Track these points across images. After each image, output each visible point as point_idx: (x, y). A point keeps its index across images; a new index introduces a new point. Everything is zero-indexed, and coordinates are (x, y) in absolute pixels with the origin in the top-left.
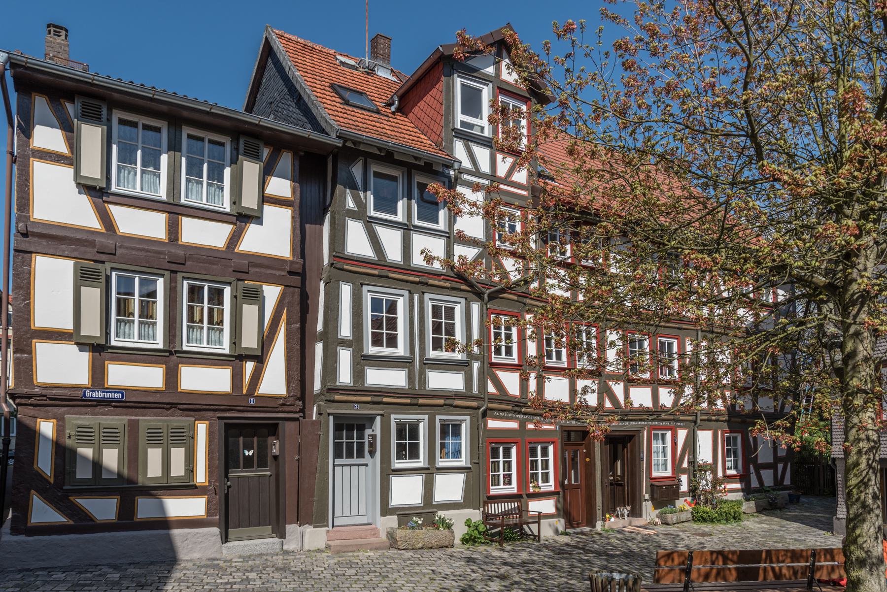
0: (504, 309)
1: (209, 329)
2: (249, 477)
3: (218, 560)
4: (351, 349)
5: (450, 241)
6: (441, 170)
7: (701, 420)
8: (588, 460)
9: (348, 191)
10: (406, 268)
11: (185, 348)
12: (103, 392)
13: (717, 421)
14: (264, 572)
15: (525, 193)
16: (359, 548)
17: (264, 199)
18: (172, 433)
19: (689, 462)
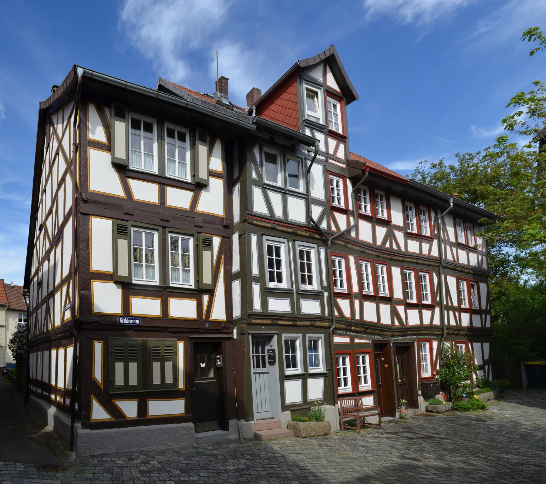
0: (338, 252)
4: (259, 284)
8: (386, 366)
10: (285, 222)
12: (129, 319)
15: (344, 166)
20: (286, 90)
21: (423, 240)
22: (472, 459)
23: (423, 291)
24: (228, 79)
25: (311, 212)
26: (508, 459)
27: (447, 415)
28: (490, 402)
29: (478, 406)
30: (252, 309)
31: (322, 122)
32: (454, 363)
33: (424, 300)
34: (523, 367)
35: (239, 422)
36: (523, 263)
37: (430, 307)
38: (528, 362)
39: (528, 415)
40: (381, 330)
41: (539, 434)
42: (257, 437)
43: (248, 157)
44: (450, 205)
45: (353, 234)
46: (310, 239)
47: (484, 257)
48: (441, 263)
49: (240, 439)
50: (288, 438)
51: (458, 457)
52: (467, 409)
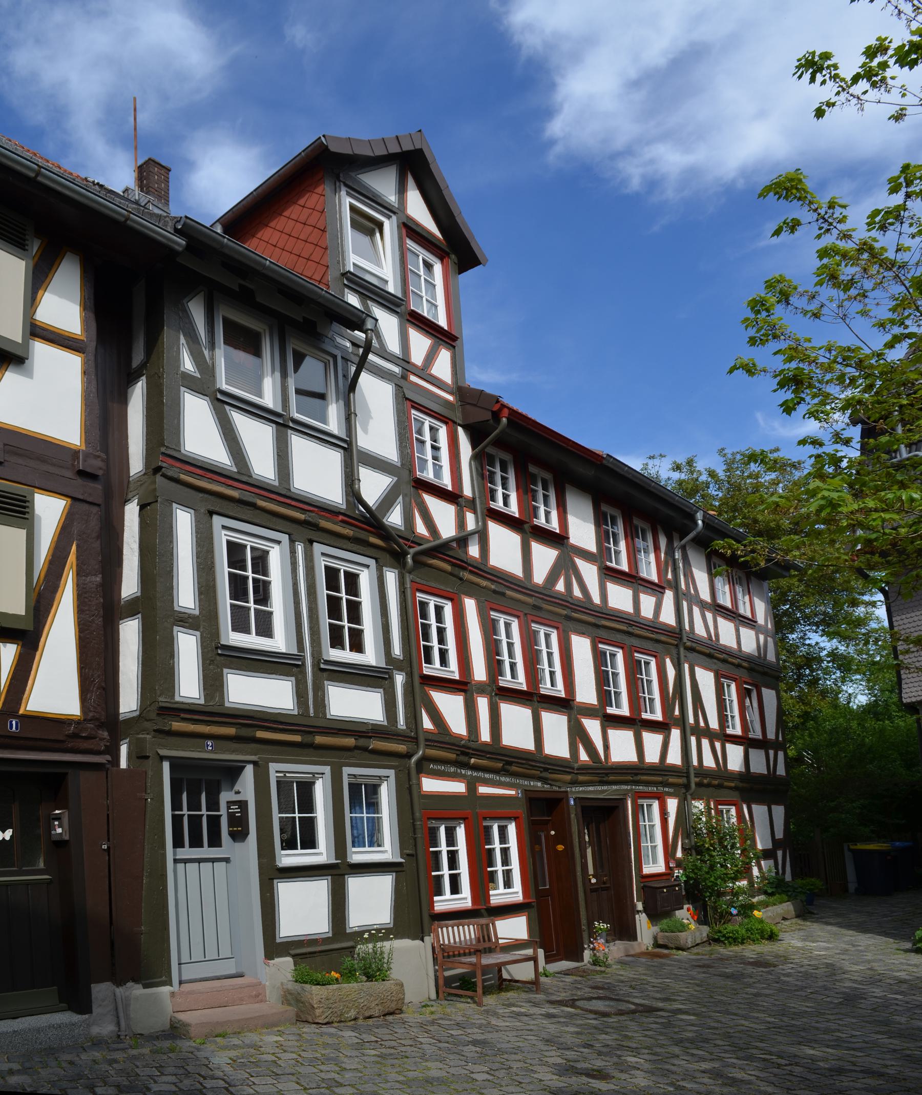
0: (433, 585)
4: (198, 633)
8: (560, 848)
10: (284, 492)
15: (450, 398)
20: (298, 200)
21: (641, 588)
22: (734, 1066)
23: (644, 693)
24: (169, 170)
25: (357, 482)
26: (813, 1059)
27: (698, 954)
28: (787, 923)
29: (762, 932)
30: (173, 695)
31: (392, 288)
32: (711, 845)
33: (646, 712)
34: (848, 855)
35: (120, 991)
36: (844, 664)
37: (661, 727)
38: (856, 845)
39: (858, 950)
40: (546, 770)
41: (878, 992)
42: (176, 1031)
43: (169, 316)
44: (696, 524)
45: (474, 551)
46: (358, 544)
47: (769, 638)
48: (681, 639)
49: (119, 1036)
50: (276, 1029)
51: (704, 1060)
52: (740, 940)
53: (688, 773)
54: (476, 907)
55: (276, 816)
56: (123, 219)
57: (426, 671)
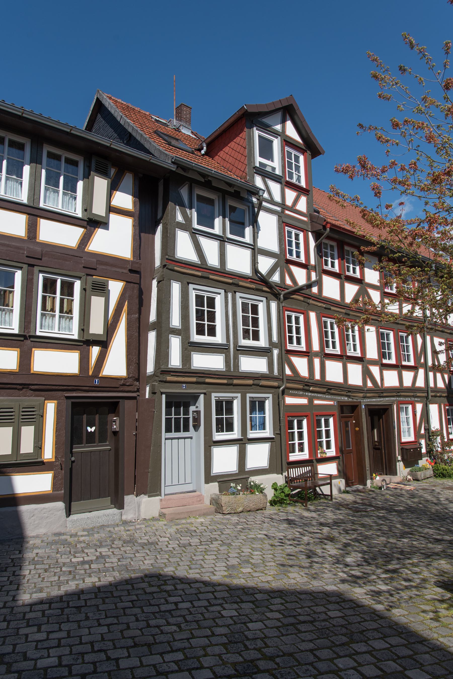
0: (294, 307)
1: (60, 317)
2: (91, 452)
3: (64, 534)
4: (180, 337)
5: (254, 252)
6: (246, 197)
7: (432, 396)
8: (357, 429)
9: (177, 207)
10: (222, 271)
11: (38, 333)
13: (440, 396)
14: (113, 546)
15: (305, 219)
16: (189, 514)
17: (111, 209)
18: (23, 412)
19: (425, 429)
37: (414, 368)
40: (349, 392)
45: (315, 290)
46: (258, 291)
53: (428, 391)
54: (311, 459)
55: (214, 417)
56: (149, 160)
57: (289, 348)
